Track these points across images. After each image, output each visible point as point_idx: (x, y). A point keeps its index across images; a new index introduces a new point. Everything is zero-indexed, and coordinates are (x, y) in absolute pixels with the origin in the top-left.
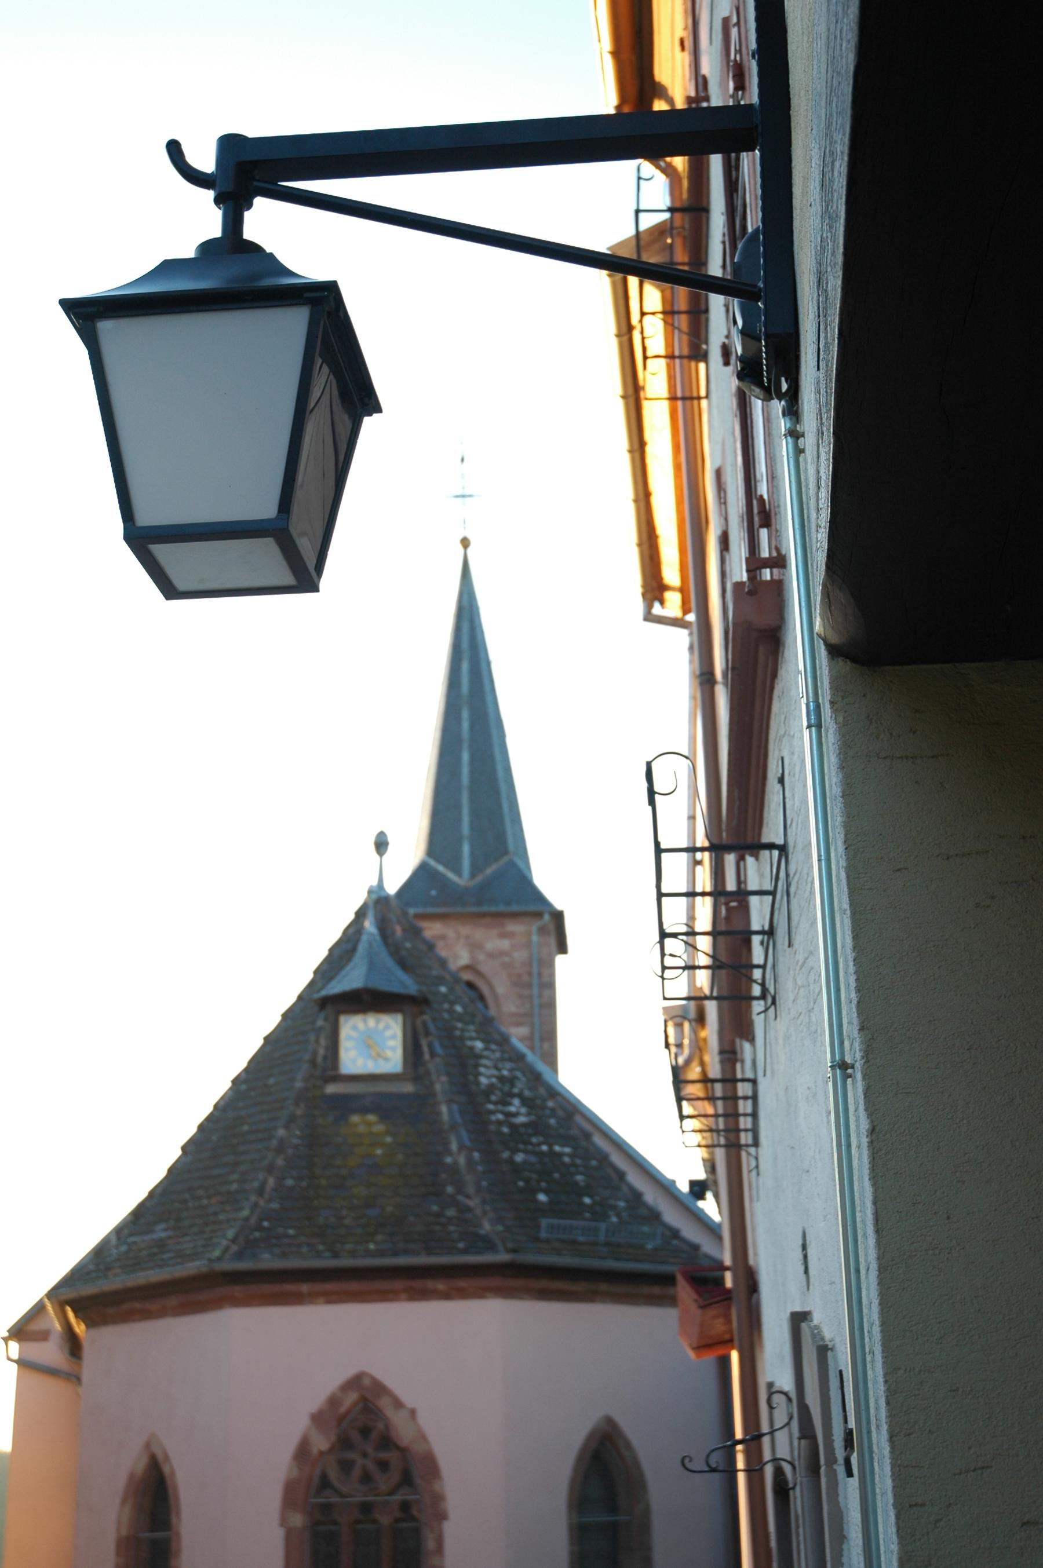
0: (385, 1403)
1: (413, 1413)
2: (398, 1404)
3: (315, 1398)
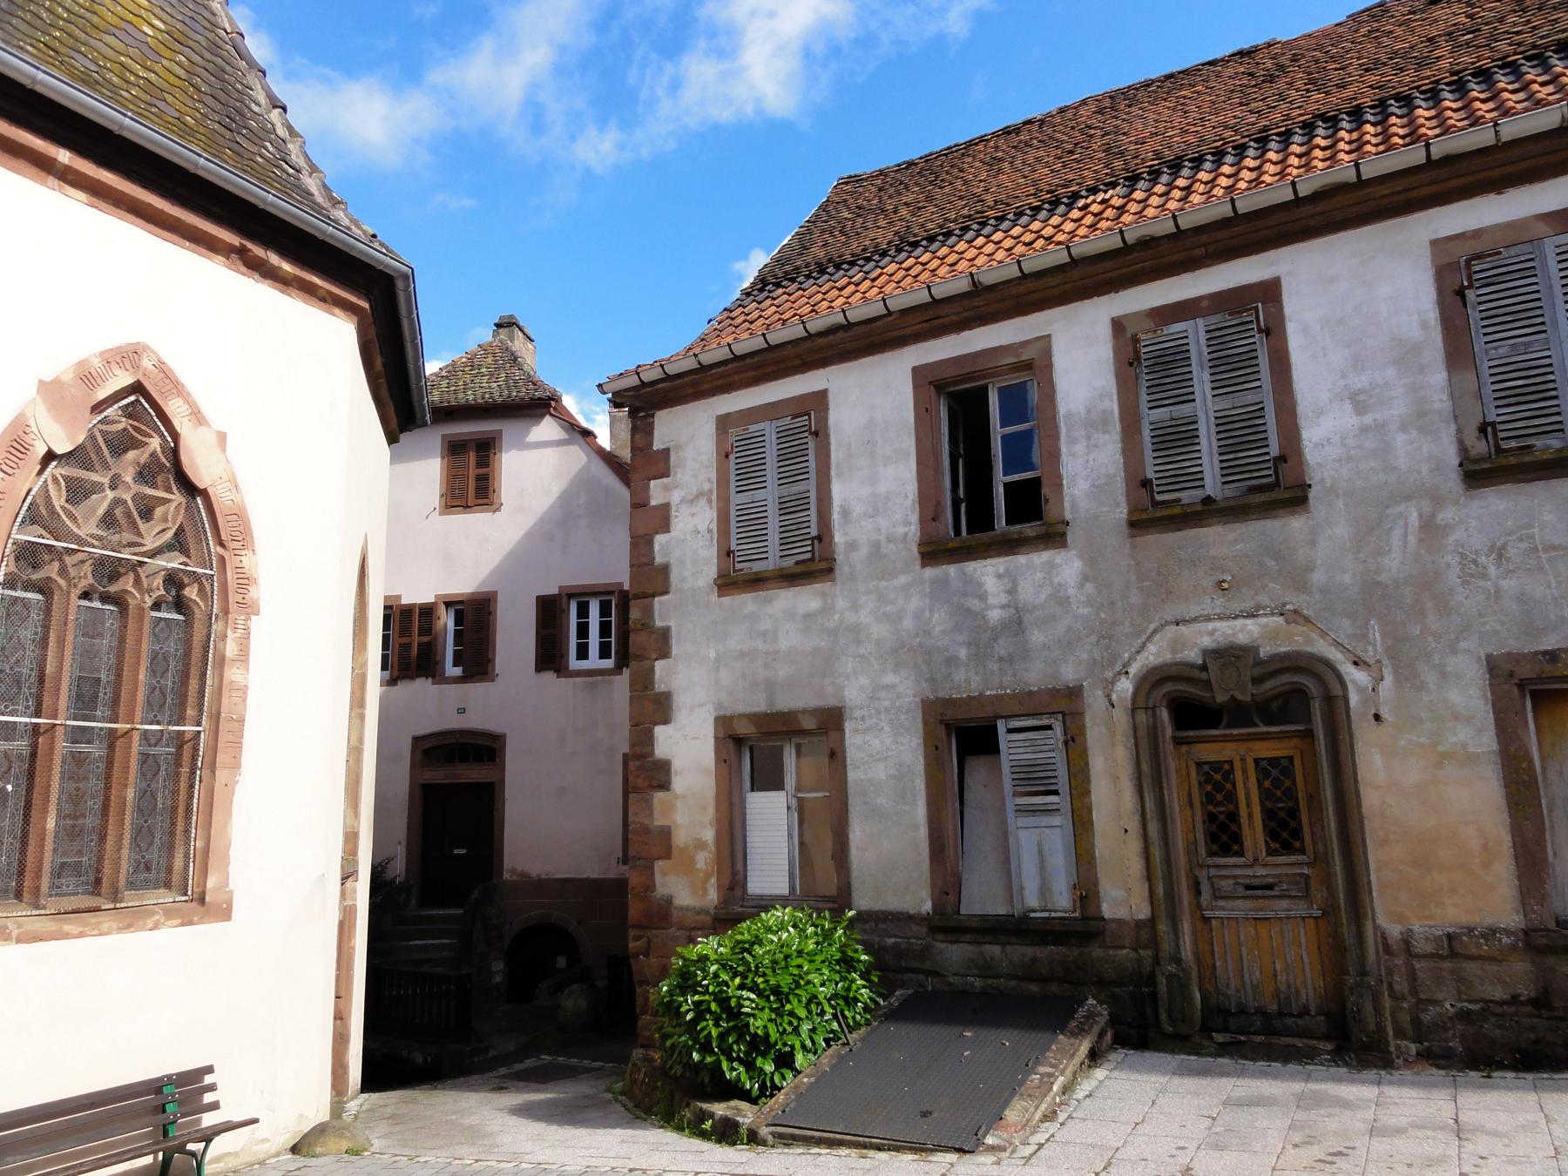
0: (175, 409)
1: (222, 438)
2: (198, 417)
3: (59, 363)
